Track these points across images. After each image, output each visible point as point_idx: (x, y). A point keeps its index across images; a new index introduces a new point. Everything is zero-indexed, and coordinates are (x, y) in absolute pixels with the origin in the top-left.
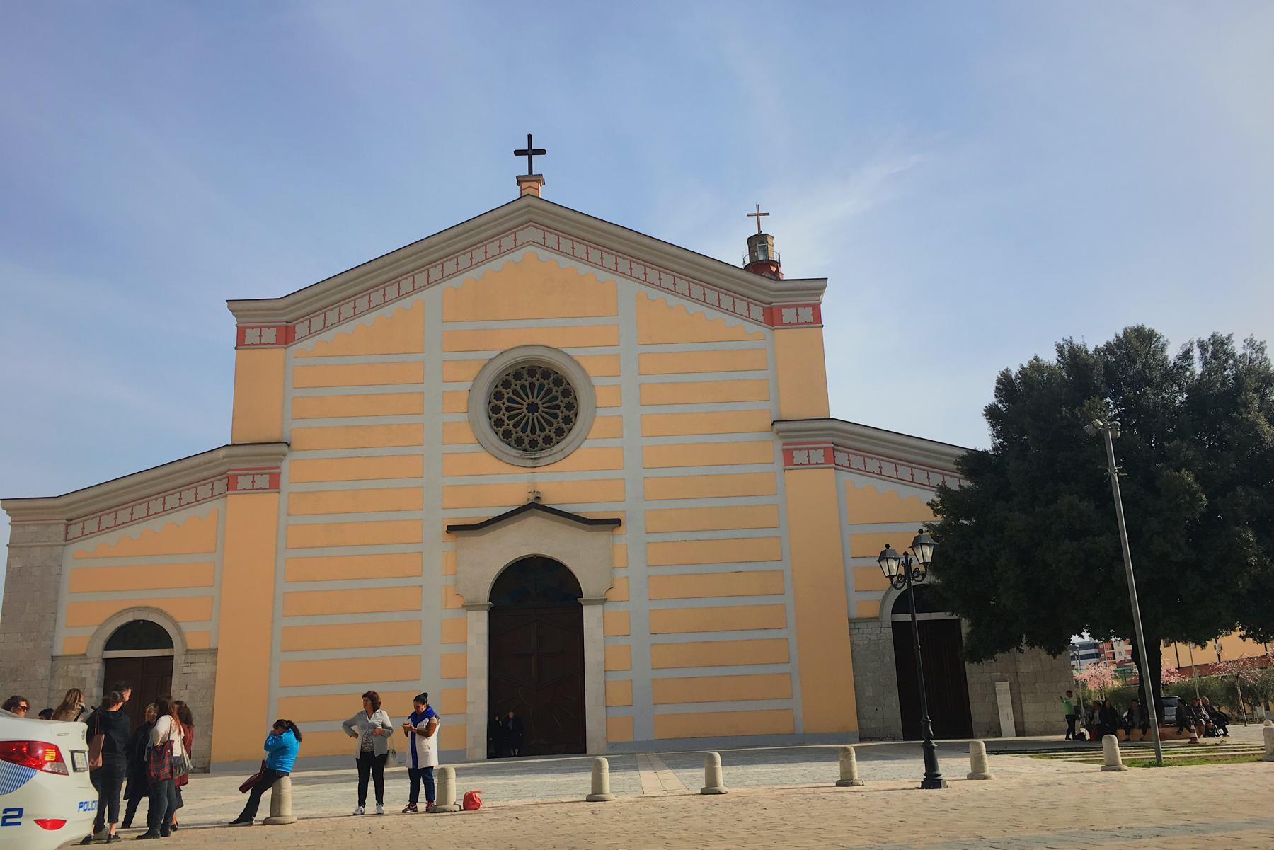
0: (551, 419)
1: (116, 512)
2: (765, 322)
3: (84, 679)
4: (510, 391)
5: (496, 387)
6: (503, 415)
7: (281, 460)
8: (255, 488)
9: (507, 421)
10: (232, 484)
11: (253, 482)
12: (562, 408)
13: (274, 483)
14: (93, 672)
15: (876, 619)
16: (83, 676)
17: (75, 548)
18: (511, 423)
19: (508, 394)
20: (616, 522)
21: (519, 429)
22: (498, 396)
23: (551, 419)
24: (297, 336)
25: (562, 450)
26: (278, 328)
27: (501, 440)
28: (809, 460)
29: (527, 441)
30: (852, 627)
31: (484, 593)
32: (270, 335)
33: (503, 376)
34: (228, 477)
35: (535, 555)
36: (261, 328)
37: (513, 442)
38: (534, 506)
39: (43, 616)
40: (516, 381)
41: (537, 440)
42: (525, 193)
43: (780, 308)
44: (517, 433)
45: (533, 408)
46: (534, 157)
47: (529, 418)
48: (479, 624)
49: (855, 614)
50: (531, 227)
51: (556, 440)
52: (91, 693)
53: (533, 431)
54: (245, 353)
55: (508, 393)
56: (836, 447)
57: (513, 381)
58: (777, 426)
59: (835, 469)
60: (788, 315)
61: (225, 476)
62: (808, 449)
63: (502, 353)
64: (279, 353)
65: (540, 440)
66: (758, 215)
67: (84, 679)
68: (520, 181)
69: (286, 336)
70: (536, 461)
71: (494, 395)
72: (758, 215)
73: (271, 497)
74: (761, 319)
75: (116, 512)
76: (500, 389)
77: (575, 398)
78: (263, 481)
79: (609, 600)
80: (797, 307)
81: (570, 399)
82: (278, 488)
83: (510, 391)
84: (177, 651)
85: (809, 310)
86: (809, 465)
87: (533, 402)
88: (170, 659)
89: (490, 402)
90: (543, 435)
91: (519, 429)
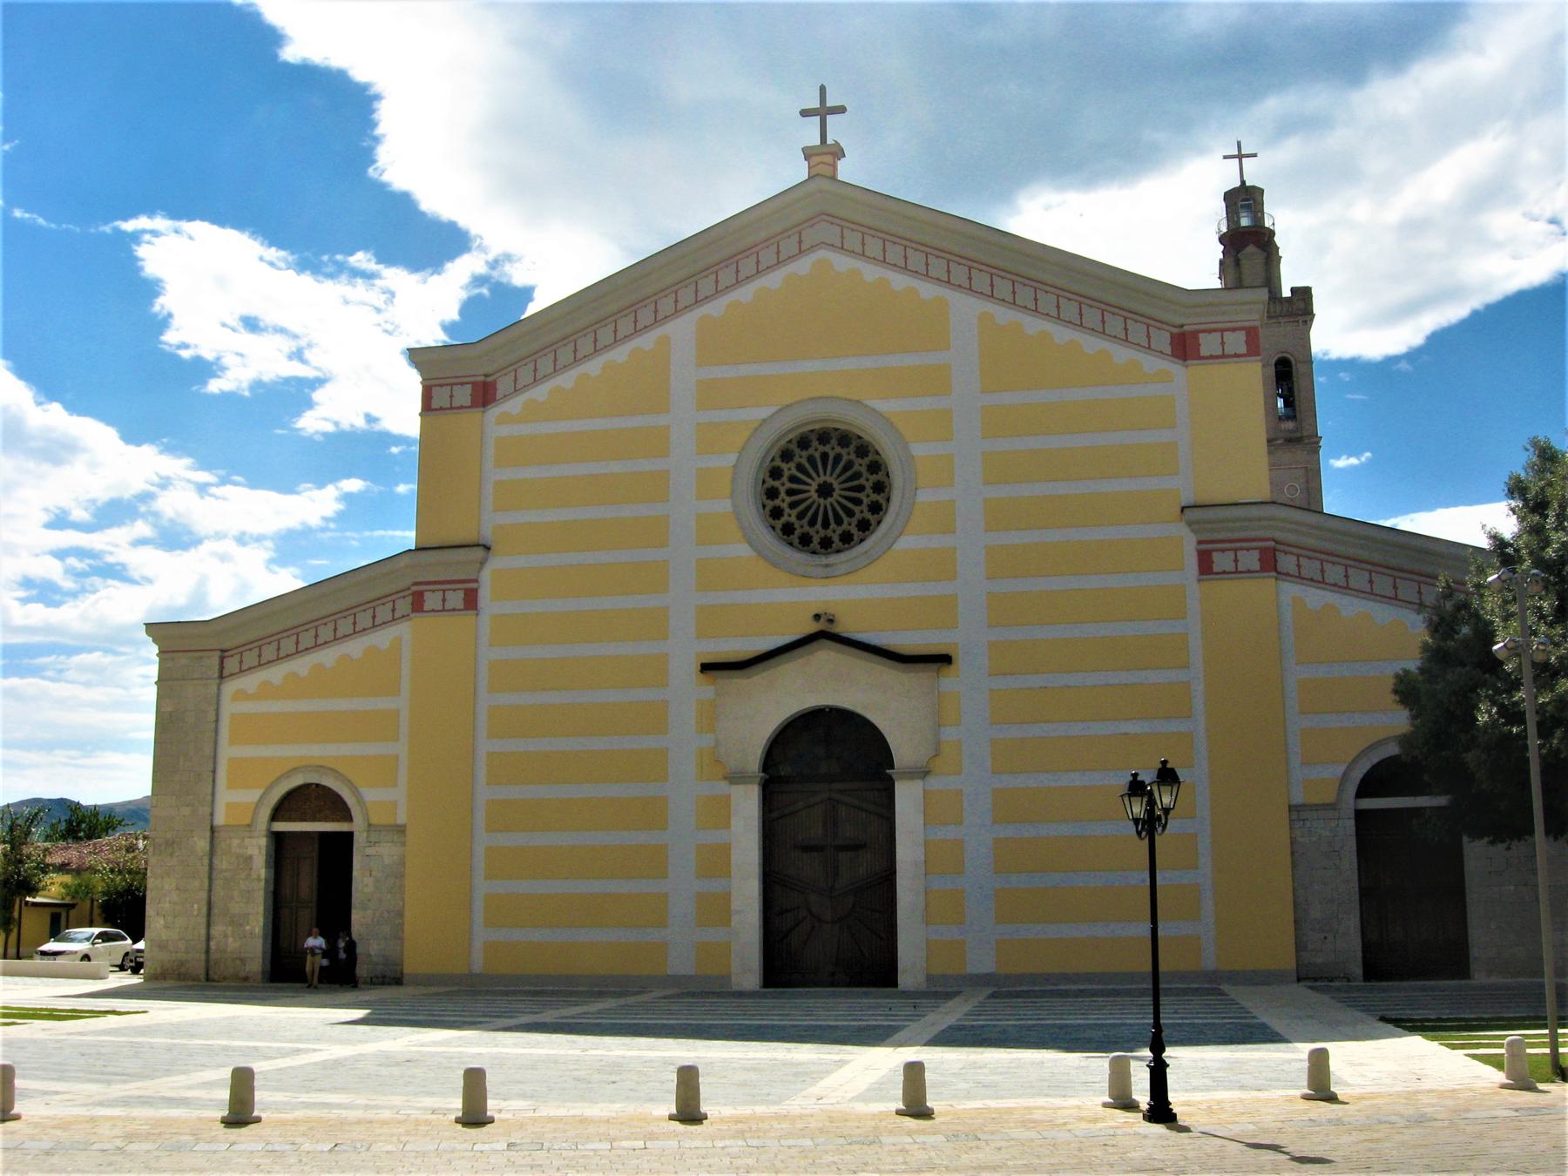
1: (241, 653)
2: (1174, 355)
3: (251, 857)
11: (444, 600)
12: (869, 490)
13: (471, 601)
14: (260, 849)
15: (1331, 806)
16: (249, 852)
17: (230, 688)
18: (794, 512)
20: (944, 659)
21: (805, 521)
22: (775, 473)
24: (499, 396)
25: (866, 552)
26: (474, 384)
30: (1294, 816)
31: (753, 759)
35: (828, 706)
36: (452, 385)
38: (825, 634)
39: (199, 775)
40: (802, 450)
42: (814, 172)
43: (1195, 334)
46: (829, 118)
48: (747, 803)
49: (1298, 798)
50: (822, 223)
52: (259, 876)
55: (789, 469)
56: (1278, 547)
57: (797, 451)
59: (1276, 579)
60: (1208, 344)
62: (1236, 550)
63: (780, 410)
64: (476, 414)
66: (1240, 157)
67: (251, 857)
68: (808, 153)
69: (485, 395)
70: (829, 569)
72: (1240, 157)
73: (469, 617)
74: (1168, 350)
75: (241, 653)
81: (880, 476)
83: (792, 465)
84: (357, 826)
88: (348, 837)
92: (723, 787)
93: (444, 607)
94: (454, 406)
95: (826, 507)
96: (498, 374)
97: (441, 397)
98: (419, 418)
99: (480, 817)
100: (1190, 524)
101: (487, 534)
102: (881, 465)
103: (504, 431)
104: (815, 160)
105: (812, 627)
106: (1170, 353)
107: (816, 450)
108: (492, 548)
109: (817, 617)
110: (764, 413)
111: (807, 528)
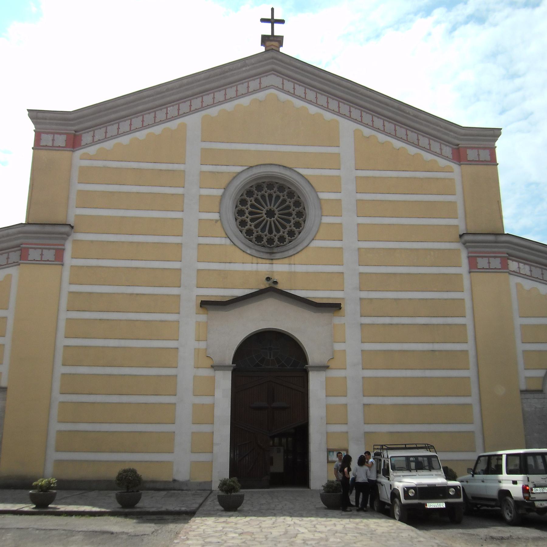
0: (287, 211)
2: (453, 159)
4: (253, 199)
5: (242, 195)
6: (247, 217)
7: (65, 239)
8: (43, 260)
9: (247, 214)
10: (24, 256)
18: (253, 224)
19: (251, 201)
21: (259, 229)
23: (287, 211)
24: (83, 143)
27: (237, 226)
28: (489, 265)
29: (265, 239)
31: (229, 359)
32: (61, 140)
33: (248, 187)
34: (21, 250)
37: (254, 239)
41: (273, 239)
42: (268, 49)
44: (257, 232)
45: (270, 213)
47: (267, 222)
50: (273, 76)
51: (289, 239)
53: (270, 232)
54: (44, 153)
58: (467, 238)
61: (18, 248)
64: (66, 154)
65: (276, 239)
71: (240, 202)
74: (450, 156)
76: (245, 197)
77: (304, 209)
78: (49, 255)
79: (330, 367)
80: (478, 148)
82: (62, 261)
83: (253, 199)
85: (487, 152)
86: (489, 270)
87: (270, 210)
89: (236, 207)
90: (278, 235)
91: (259, 229)
92: (209, 372)
93: (41, 259)
94: (54, 145)
95: (270, 223)
96: (83, 132)
97: (47, 139)
98: (32, 150)
99: (55, 412)
100: (464, 244)
101: (71, 221)
102: (300, 203)
103: (86, 163)
104: (268, 43)
105: (264, 285)
106: (452, 158)
107: (266, 192)
108: (74, 227)
109: (268, 279)
110: (239, 169)
111: (293, 207)
